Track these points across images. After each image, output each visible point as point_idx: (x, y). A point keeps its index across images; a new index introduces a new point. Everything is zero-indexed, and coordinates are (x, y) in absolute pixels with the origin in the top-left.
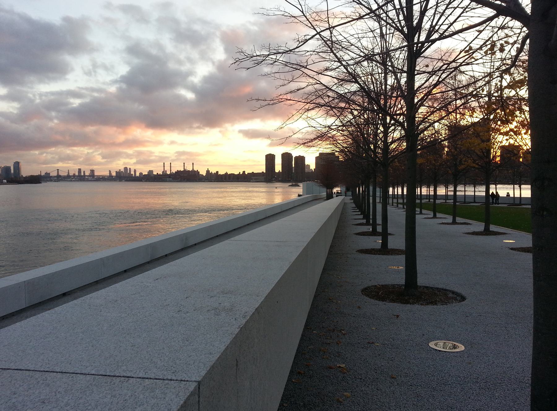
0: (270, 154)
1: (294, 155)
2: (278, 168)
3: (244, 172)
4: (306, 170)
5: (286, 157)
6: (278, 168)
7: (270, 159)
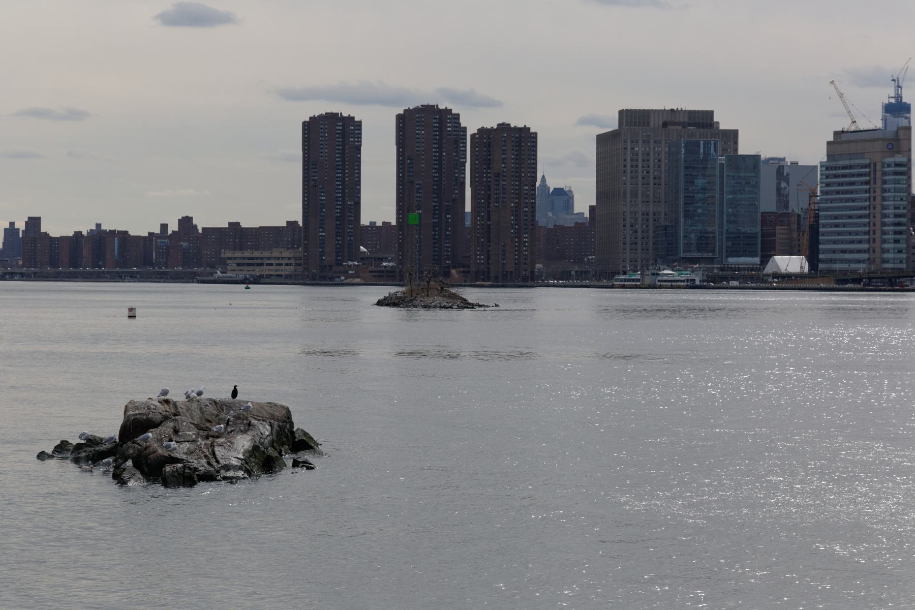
0: (332, 118)
1: (472, 122)
2: (378, 202)
3: (33, 223)
4: (545, 218)
5: (426, 132)
6: (378, 202)
7: (330, 145)
